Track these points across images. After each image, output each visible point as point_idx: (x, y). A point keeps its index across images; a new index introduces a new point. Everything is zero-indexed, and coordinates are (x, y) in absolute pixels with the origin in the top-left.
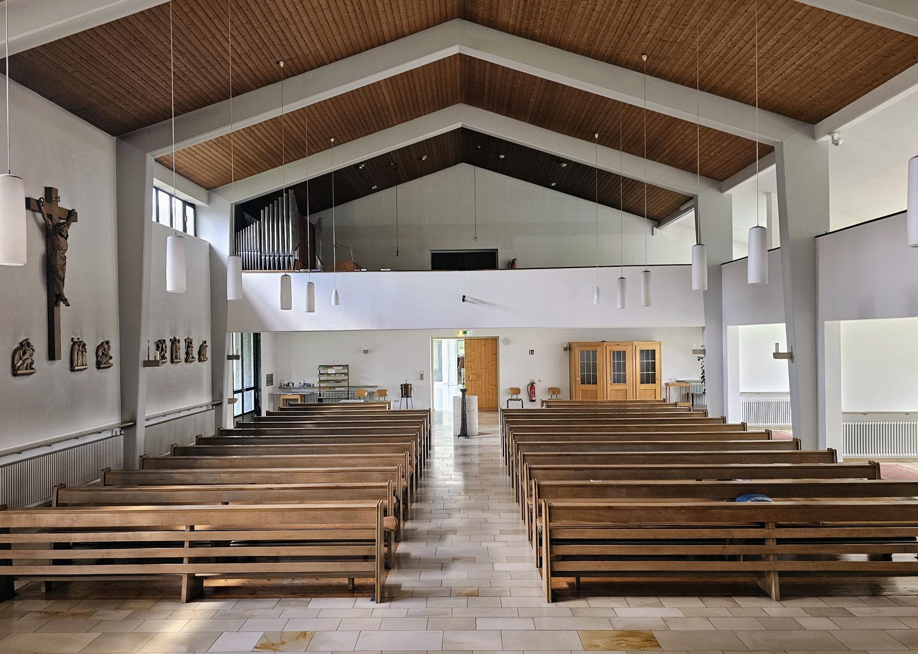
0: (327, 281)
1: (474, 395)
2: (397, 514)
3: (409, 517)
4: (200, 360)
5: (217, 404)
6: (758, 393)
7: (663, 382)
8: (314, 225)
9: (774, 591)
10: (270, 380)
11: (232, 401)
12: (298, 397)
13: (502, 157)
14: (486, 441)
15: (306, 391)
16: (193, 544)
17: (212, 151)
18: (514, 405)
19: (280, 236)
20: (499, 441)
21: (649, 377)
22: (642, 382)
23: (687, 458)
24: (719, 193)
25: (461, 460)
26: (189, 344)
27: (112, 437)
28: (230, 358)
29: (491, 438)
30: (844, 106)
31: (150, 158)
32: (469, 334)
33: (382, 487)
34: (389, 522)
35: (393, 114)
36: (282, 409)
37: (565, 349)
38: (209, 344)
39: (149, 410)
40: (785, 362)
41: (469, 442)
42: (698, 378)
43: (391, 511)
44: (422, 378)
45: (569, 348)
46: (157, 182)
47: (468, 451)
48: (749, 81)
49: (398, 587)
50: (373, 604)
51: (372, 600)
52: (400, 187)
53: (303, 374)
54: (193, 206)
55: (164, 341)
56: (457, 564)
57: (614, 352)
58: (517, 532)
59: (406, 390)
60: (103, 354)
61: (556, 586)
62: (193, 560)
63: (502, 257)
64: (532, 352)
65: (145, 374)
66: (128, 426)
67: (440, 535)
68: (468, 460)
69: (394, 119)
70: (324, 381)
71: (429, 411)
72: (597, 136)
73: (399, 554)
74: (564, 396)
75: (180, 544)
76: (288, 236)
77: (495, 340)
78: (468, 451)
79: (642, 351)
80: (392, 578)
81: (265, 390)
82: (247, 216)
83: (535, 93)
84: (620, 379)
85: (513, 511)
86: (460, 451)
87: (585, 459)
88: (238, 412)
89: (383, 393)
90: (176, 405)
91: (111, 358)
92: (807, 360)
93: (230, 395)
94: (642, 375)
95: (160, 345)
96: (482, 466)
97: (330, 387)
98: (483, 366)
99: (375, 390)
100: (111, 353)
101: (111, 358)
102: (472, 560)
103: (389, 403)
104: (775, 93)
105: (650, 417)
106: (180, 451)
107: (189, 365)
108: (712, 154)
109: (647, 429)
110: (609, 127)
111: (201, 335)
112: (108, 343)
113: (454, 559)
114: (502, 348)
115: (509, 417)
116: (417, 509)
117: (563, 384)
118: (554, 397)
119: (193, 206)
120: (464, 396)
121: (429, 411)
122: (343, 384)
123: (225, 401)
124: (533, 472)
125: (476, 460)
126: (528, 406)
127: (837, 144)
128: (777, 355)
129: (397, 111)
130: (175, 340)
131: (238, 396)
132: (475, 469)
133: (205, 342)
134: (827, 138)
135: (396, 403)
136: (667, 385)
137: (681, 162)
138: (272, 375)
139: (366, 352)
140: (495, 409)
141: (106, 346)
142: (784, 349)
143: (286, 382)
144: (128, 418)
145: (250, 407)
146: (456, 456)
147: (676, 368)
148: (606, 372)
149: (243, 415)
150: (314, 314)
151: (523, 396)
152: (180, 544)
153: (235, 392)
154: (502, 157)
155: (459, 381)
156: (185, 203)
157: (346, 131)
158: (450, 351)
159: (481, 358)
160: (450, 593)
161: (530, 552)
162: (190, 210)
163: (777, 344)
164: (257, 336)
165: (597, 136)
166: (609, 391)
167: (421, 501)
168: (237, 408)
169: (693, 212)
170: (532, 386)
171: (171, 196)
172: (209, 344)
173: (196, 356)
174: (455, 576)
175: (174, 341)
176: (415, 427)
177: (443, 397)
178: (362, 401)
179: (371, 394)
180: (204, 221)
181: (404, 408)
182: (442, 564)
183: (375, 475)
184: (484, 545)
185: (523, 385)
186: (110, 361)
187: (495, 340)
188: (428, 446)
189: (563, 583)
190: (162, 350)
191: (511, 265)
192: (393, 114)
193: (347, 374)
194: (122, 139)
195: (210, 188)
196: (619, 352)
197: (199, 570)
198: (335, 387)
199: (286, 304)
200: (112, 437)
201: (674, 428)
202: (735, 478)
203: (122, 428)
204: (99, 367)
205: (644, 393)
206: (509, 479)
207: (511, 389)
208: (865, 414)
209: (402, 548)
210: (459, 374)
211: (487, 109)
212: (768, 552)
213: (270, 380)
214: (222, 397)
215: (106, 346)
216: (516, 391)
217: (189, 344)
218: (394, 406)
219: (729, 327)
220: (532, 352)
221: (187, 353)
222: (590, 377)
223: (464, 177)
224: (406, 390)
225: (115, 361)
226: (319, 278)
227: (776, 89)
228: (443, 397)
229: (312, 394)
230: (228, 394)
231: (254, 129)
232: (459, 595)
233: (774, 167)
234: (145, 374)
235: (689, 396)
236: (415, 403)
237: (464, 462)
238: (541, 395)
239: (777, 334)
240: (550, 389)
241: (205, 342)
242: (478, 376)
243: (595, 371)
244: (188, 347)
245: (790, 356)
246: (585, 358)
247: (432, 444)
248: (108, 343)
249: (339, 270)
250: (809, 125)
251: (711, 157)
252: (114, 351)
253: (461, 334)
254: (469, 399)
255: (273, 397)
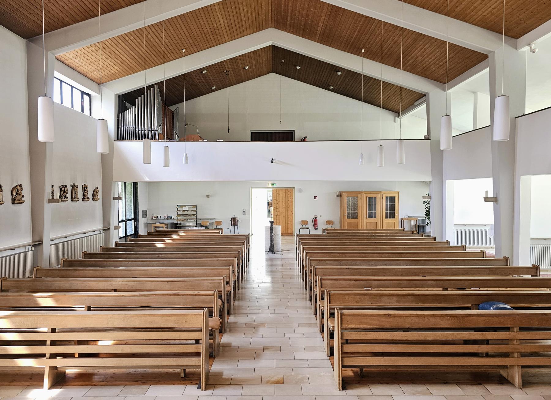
0: (177, 147)
1: (278, 225)
2: (221, 316)
3: (232, 312)
4: (93, 200)
5: (106, 230)
6: (465, 225)
7: (400, 217)
8: (169, 109)
9: (517, 380)
10: (145, 214)
11: (117, 228)
12: (164, 225)
13: (298, 68)
14: (286, 255)
15: (169, 222)
16: (54, 343)
17: (108, 61)
18: (304, 232)
19: (148, 116)
20: (295, 256)
21: (391, 213)
22: (387, 217)
23: (433, 271)
24: (443, 92)
25: (270, 269)
26: (85, 188)
27: (25, 252)
28: (115, 198)
29: (290, 251)
30: (542, 23)
31: (51, 56)
32: (277, 186)
33: (209, 295)
34: (214, 322)
35: (225, 33)
36: (149, 233)
37: (337, 196)
38: (100, 189)
39: (52, 234)
40: (492, 204)
41: (276, 256)
42: (423, 214)
43: (216, 312)
44: (244, 214)
45: (340, 195)
46: (57, 74)
47: (275, 262)
48: (475, 5)
49: (219, 375)
50: (199, 392)
51: (199, 387)
52: (231, 88)
53: (167, 210)
54: (89, 95)
55: (66, 186)
56: (267, 354)
57: (369, 198)
58: (310, 325)
59: (234, 222)
60: (17, 194)
61: (345, 375)
62: (53, 356)
63: (297, 135)
64: (316, 198)
65: (48, 208)
66: (37, 244)
67: (254, 327)
68: (274, 269)
69: (226, 37)
70: (180, 215)
71: (248, 235)
72: (363, 51)
73: (223, 344)
74: (337, 226)
75: (43, 343)
76: (154, 117)
77: (292, 189)
78: (275, 262)
79: (387, 198)
80: (216, 367)
81: (142, 221)
82: (127, 104)
83: (322, 18)
84: (372, 215)
85: (306, 308)
86: (269, 262)
87: (359, 272)
88: (122, 234)
89: (219, 223)
90: (76, 229)
91: (23, 196)
92: (506, 202)
93: (116, 223)
94: (386, 213)
95: (63, 189)
96: (283, 273)
97: (185, 219)
98: (284, 206)
99: (214, 221)
100: (23, 193)
101: (23, 196)
102: (278, 349)
103: (222, 230)
104: (493, 14)
105: (392, 239)
106: (69, 264)
107: (85, 203)
108: (441, 63)
109: (398, 249)
110: (372, 44)
111: (95, 182)
112: (20, 186)
113: (265, 349)
114: (297, 195)
115: (302, 239)
116: (235, 323)
117: (335, 218)
118: (330, 226)
119: (89, 95)
120: (272, 226)
121: (248, 235)
122: (192, 217)
123: (112, 228)
124: (323, 282)
125: (279, 268)
126: (313, 232)
127: (534, 52)
128: (486, 199)
129: (228, 31)
130: (74, 185)
131: (121, 224)
132: (279, 275)
133: (97, 188)
134: (526, 49)
135: (227, 229)
136: (402, 219)
137: (419, 70)
138: (146, 211)
139: (208, 196)
140: (292, 235)
141: (19, 188)
142: (491, 195)
143: (155, 216)
144: (37, 239)
145: (131, 231)
146: (267, 266)
147: (409, 208)
148: (363, 211)
149: (126, 236)
150: (167, 166)
151: (310, 226)
152: (43, 343)
153: (120, 222)
154: (298, 68)
155: (268, 216)
156: (83, 93)
157: (193, 45)
158: (261, 197)
159: (283, 202)
160: (260, 381)
161: (323, 343)
162: (86, 98)
163: (487, 192)
164: (135, 185)
165: (363, 51)
166: (365, 223)
167: (242, 299)
168: (120, 232)
169: (425, 105)
170: (316, 219)
171: (72, 87)
172: (100, 189)
173: (90, 196)
174: (266, 365)
175: (74, 186)
176: (235, 250)
177: (258, 227)
178: (204, 228)
179: (211, 224)
180: (96, 104)
181: (232, 233)
182: (255, 354)
183: (206, 283)
184: (287, 336)
185: (310, 219)
186: (23, 199)
187: (292, 189)
188: (247, 258)
189: (349, 372)
190: (64, 192)
191: (304, 140)
192: (225, 33)
193: (196, 211)
194: (31, 41)
195: (99, 83)
196: (372, 198)
197: (59, 362)
198: (187, 219)
199: (147, 160)
200: (25, 252)
201: (405, 249)
202: (469, 288)
203: (33, 246)
204: (13, 203)
205: (387, 224)
206: (302, 283)
207: (302, 221)
208: (545, 239)
209: (225, 339)
210: (269, 212)
211: (289, 32)
212: (513, 351)
213: (145, 214)
214: (109, 225)
215: (19, 188)
216: (305, 223)
217: (85, 188)
218: (226, 232)
219: (523, 177)
220: (316, 198)
221: (84, 195)
222: (353, 215)
223: (273, 82)
224: (234, 222)
225: (27, 198)
226: (175, 146)
227: (494, 11)
228: (258, 227)
229: (173, 223)
230: (114, 222)
231: (125, 36)
232: (268, 383)
233: (487, 70)
234: (48, 208)
235: (415, 227)
236: (241, 230)
237: (272, 269)
238: (322, 226)
239: (486, 185)
240: (327, 221)
241: (97, 188)
242: (281, 213)
243: (356, 210)
244: (85, 190)
245: (495, 200)
246: (350, 201)
247: (250, 257)
248: (20, 186)
249: (188, 140)
250: (514, 40)
251: (440, 66)
252: (26, 192)
253: (270, 186)
254: (275, 228)
255: (147, 225)
